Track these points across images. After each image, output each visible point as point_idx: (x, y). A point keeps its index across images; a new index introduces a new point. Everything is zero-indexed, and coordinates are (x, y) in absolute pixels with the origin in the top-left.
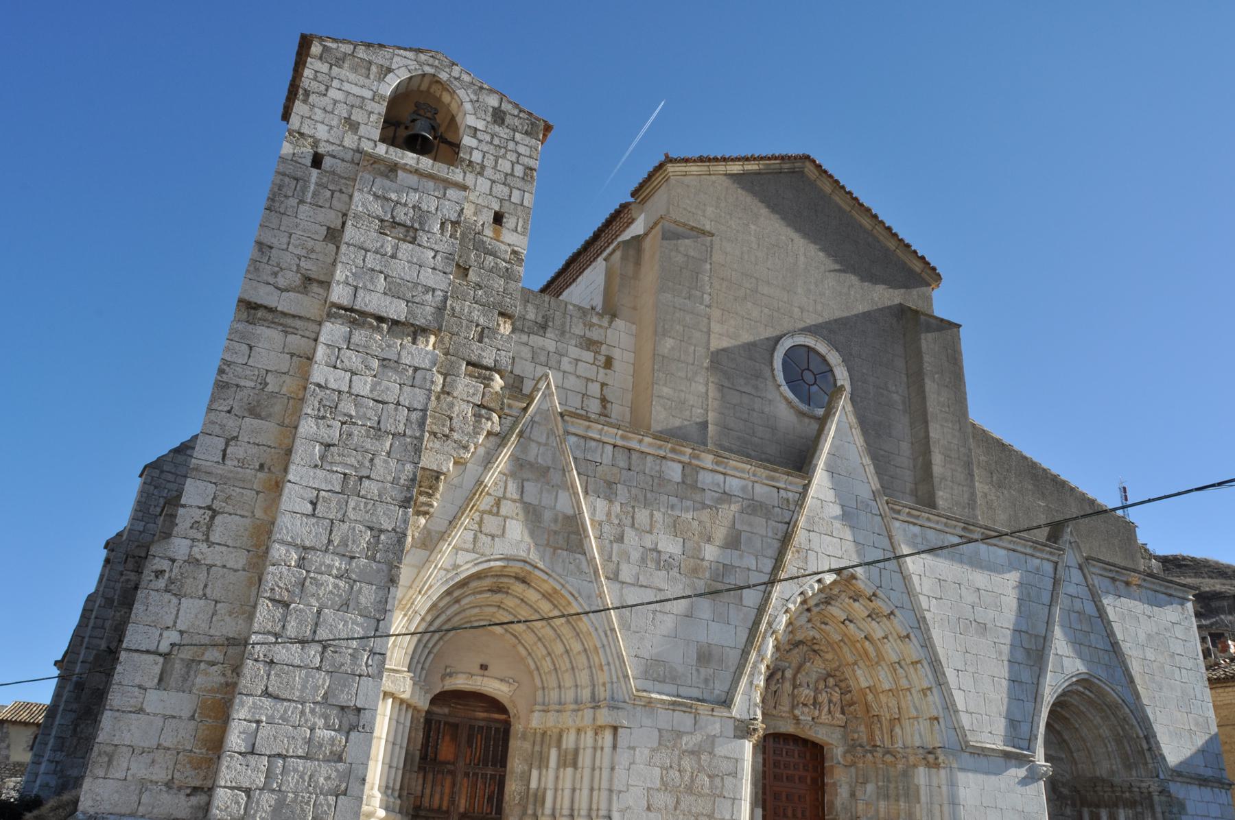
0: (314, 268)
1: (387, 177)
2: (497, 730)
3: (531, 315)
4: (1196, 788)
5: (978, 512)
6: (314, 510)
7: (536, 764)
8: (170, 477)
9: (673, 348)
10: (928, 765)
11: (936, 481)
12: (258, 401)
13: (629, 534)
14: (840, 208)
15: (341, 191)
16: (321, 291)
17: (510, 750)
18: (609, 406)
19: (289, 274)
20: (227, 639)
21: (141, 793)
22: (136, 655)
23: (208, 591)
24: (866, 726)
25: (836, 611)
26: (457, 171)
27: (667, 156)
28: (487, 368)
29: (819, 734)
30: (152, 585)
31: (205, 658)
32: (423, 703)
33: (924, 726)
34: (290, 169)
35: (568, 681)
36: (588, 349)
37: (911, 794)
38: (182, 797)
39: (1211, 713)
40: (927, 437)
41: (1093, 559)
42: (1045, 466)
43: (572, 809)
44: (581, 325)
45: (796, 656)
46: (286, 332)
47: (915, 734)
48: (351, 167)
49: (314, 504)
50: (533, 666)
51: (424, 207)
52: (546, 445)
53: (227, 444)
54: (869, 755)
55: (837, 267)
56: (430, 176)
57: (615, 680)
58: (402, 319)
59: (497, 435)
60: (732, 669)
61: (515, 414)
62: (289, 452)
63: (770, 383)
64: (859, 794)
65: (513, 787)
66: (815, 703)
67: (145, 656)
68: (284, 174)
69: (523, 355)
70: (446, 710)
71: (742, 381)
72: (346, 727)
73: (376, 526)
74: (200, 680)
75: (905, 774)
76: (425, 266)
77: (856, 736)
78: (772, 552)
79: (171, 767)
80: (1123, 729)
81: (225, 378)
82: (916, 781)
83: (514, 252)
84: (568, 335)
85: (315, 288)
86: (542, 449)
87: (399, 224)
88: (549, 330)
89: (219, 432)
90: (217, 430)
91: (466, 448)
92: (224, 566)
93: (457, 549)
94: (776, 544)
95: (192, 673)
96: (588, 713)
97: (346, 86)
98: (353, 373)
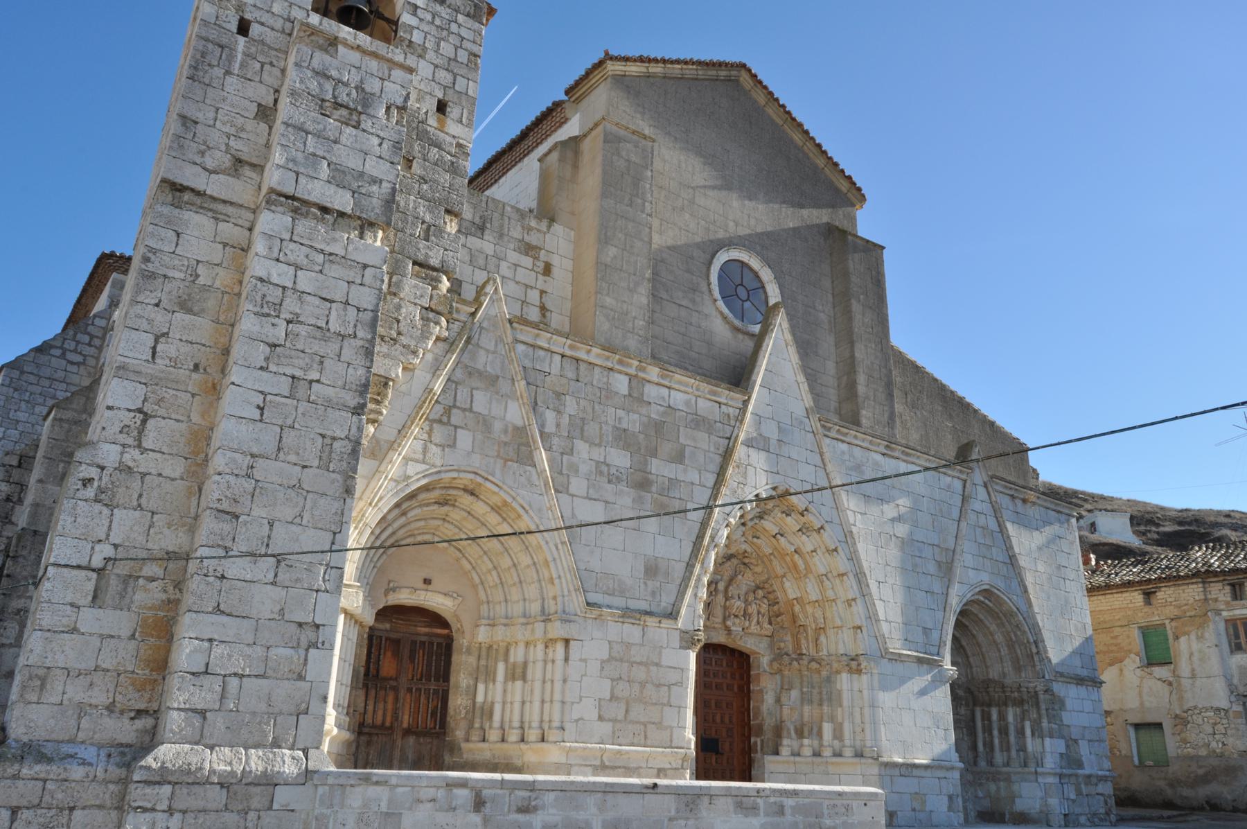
0: (245, 149)
1: (326, 51)
2: (439, 644)
4: (1073, 687)
5: (897, 431)
6: (262, 415)
7: (482, 678)
8: (32, 379)
9: (615, 257)
10: (851, 671)
11: (860, 400)
12: (189, 295)
13: (581, 447)
14: (773, 122)
15: (271, 64)
16: (254, 175)
17: (453, 667)
18: (548, 314)
19: (218, 154)
20: (167, 553)
21: (80, 718)
22: (66, 570)
23: (143, 501)
24: (792, 635)
25: (769, 525)
26: (398, 51)
27: (607, 53)
28: (434, 269)
29: (748, 644)
30: (80, 495)
31: (143, 573)
32: (370, 619)
33: (847, 635)
34: (213, 34)
35: (515, 594)
36: (527, 254)
37: (833, 698)
38: (126, 721)
39: (1088, 620)
40: (852, 357)
41: (997, 478)
42: (952, 388)
43: (522, 722)
44: (519, 228)
45: (729, 568)
46: (216, 219)
47: (839, 643)
48: (282, 37)
49: (261, 409)
50: (477, 580)
51: (368, 88)
52: (494, 352)
53: (156, 341)
54: (795, 663)
55: (719, 183)
56: (374, 55)
57: (566, 593)
58: (348, 210)
59: (445, 340)
60: (678, 582)
62: (226, 352)
63: (706, 297)
64: (784, 699)
65: (458, 702)
66: (746, 614)
67: (76, 572)
68: (207, 40)
70: (388, 626)
71: (680, 294)
72: (304, 643)
73: (329, 433)
74: (139, 597)
75: (828, 680)
76: (368, 150)
77: (782, 645)
78: (714, 467)
79: (112, 689)
80: (1016, 635)
81: (151, 267)
82: (838, 687)
83: (459, 145)
84: (506, 239)
85: (247, 171)
86: (490, 356)
87: (341, 106)
88: (487, 232)
89: (147, 328)
90: (144, 325)
91: (415, 353)
92: (160, 475)
93: (407, 460)
94: (718, 459)
95: (130, 589)
96: (539, 627)
98: (298, 268)
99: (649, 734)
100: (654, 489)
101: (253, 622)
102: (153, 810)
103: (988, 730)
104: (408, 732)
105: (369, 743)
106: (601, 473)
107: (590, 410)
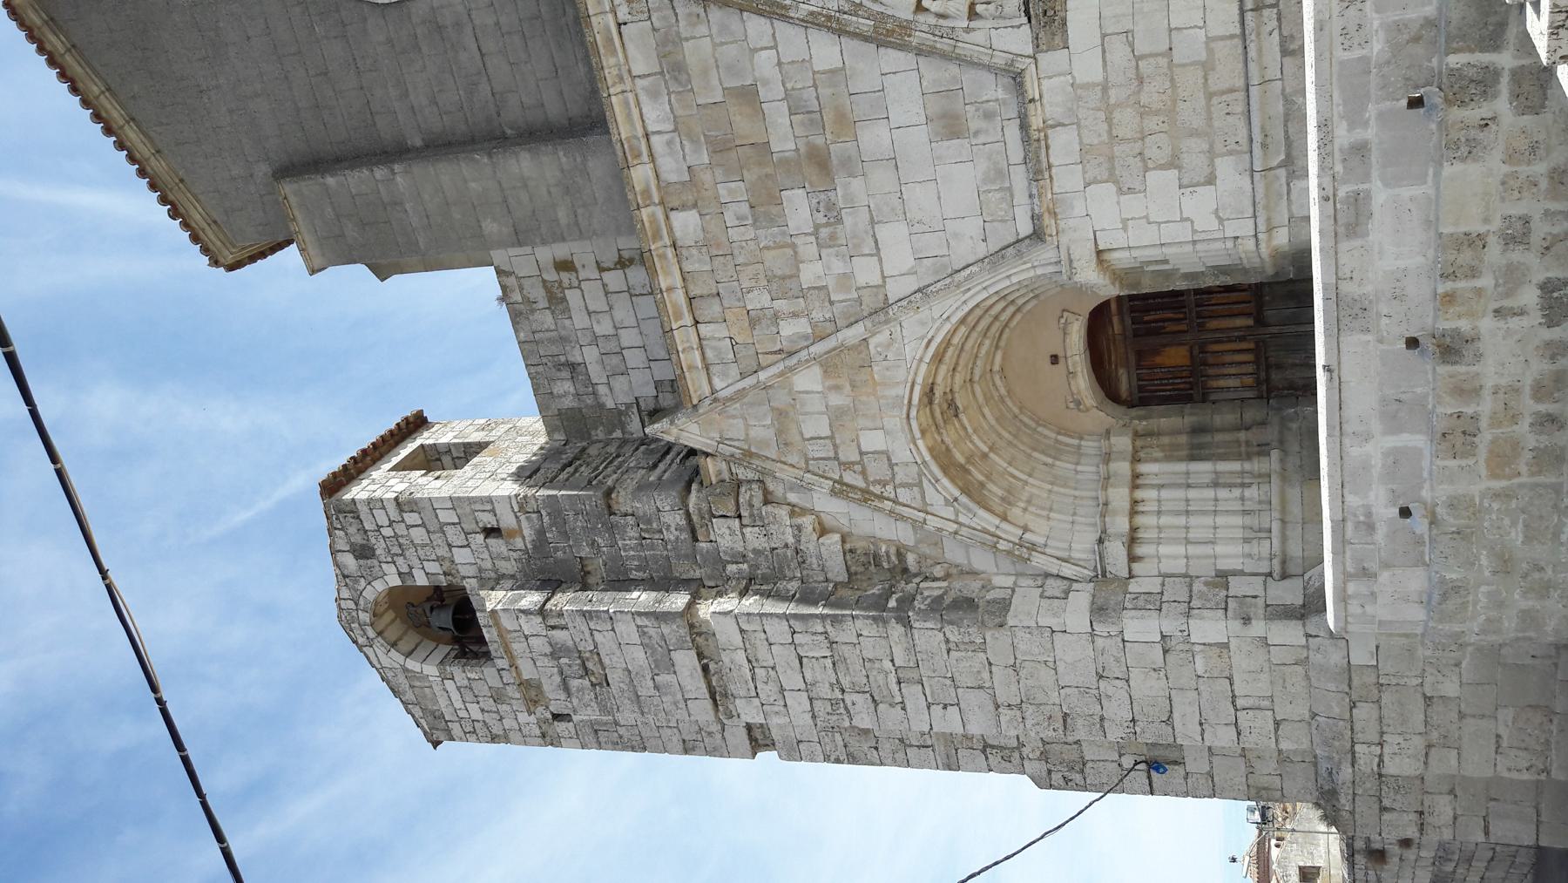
3: (568, 386)
18: (626, 255)
44: (537, 316)
70: (1122, 371)
88: (571, 359)
97: (458, 704)
101: (1173, 693)
102: (1381, 756)
104: (1260, 321)
105: (1279, 367)
106: (833, 237)
107: (750, 270)
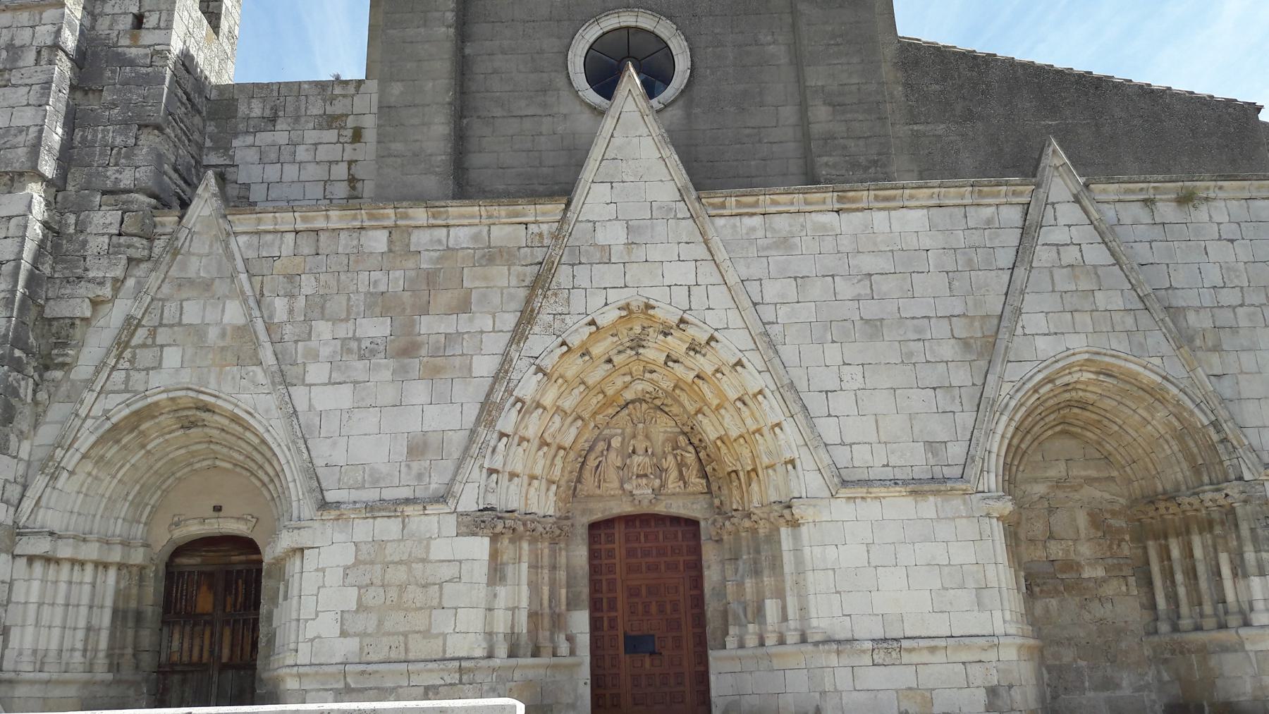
3: (257, 112)
18: (359, 185)
36: (330, 128)
60: (456, 455)
61: (169, 230)
63: (565, 94)
69: (249, 159)
84: (303, 120)
88: (279, 121)
99: (411, 646)
100: (423, 352)
103: (1169, 575)
104: (224, 667)
105: (184, 681)
106: (349, 351)
107: (333, 283)
